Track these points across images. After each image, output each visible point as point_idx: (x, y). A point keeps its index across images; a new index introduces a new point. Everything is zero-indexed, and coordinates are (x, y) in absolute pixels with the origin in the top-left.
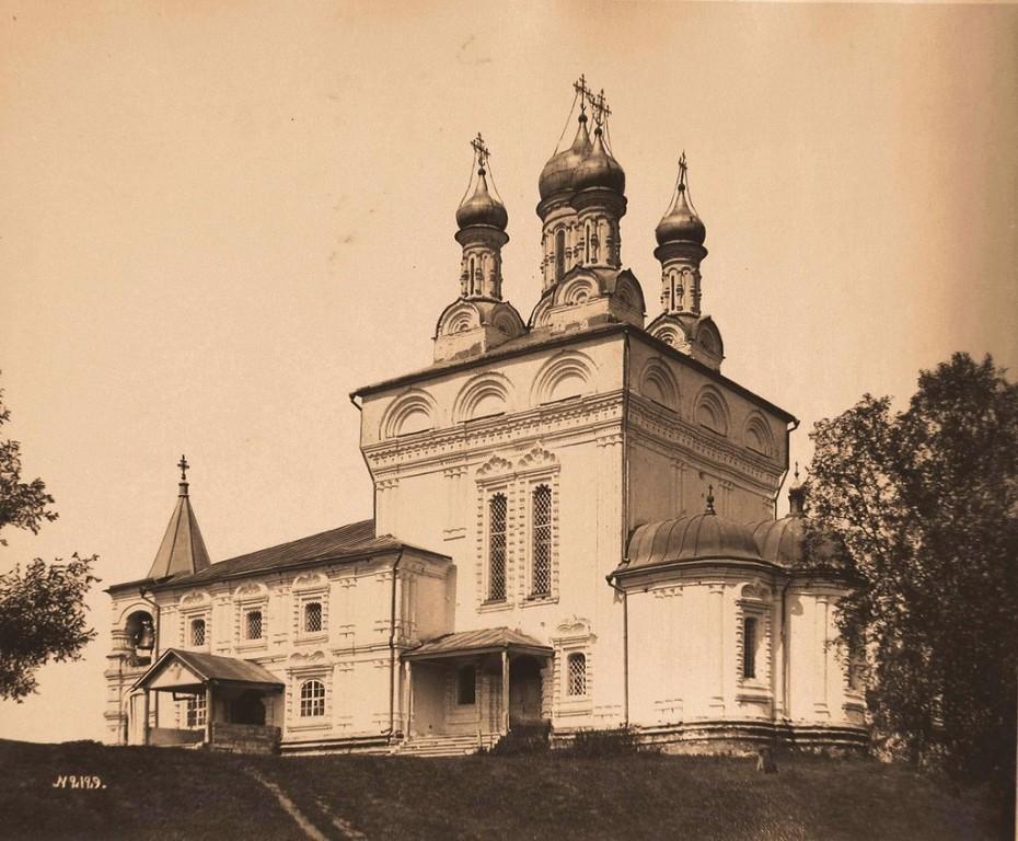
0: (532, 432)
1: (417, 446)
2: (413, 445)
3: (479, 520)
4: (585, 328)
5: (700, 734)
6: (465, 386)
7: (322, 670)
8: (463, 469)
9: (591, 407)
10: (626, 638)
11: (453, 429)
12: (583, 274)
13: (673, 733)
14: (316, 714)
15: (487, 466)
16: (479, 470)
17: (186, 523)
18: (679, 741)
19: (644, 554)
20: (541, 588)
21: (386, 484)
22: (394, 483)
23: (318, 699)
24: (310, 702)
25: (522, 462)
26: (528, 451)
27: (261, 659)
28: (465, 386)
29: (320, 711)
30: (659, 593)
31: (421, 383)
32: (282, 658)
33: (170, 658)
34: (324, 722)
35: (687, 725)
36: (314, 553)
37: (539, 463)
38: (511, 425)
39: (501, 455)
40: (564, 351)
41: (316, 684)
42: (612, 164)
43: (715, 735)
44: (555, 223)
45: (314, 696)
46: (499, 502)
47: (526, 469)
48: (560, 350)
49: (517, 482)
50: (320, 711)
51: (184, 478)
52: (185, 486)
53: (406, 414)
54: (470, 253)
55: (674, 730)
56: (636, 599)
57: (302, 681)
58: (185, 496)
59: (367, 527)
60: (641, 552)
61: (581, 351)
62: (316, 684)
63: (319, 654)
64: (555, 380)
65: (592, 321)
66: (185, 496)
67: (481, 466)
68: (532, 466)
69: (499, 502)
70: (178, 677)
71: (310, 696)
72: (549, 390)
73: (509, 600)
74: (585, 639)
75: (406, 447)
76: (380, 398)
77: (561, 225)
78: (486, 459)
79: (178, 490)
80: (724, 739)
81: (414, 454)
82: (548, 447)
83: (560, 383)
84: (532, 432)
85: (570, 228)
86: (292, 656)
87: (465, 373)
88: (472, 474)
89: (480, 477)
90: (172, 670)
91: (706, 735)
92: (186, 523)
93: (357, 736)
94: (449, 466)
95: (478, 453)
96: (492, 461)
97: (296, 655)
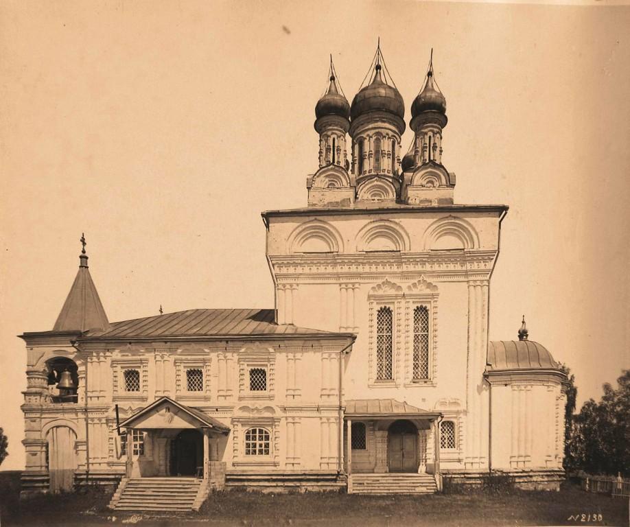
0: (419, 268)
1: (288, 263)
2: (315, 262)
3: (370, 323)
4: (435, 205)
5: (542, 478)
6: (365, 226)
7: (273, 421)
8: (357, 285)
9: (340, 261)
10: (490, 414)
11: (354, 255)
12: (434, 168)
13: (526, 476)
14: (261, 452)
15: (379, 286)
16: (373, 288)
17: (83, 290)
18: (531, 482)
19: (501, 361)
20: (422, 373)
21: (288, 286)
22: (295, 286)
23: (263, 442)
24: (255, 446)
25: (409, 287)
26: (380, 281)
27: (204, 408)
28: (365, 226)
29: (265, 450)
30: (515, 388)
31: (329, 217)
32: (230, 409)
33: (164, 403)
34: (272, 460)
35: (535, 472)
36: (176, 329)
37: (422, 290)
38: (403, 260)
39: (393, 281)
40: (316, 219)
41: (261, 431)
42: (443, 105)
43: (550, 479)
44: (374, 131)
45: (258, 438)
46: (385, 313)
47: (376, 293)
48: (448, 214)
49: (403, 301)
50: (265, 450)
51: (84, 252)
52: (84, 258)
53: (306, 238)
54: (333, 133)
55: (527, 474)
56: (500, 392)
57: (247, 428)
58: (84, 265)
59: (268, 316)
60: (498, 359)
61: (331, 223)
62: (261, 431)
63: (269, 409)
64: (439, 235)
65: (440, 201)
66: (84, 265)
67: (375, 285)
68: (415, 291)
69: (385, 313)
70: (171, 421)
71: (254, 438)
72: (436, 238)
73: (398, 382)
74: (458, 412)
75: (285, 262)
76: (359, 219)
77: (377, 134)
78: (380, 281)
79: (78, 262)
80: (554, 481)
81: (374, 267)
82: (397, 281)
83: (441, 238)
84: (419, 268)
85: (385, 137)
86: (240, 409)
87: (367, 216)
88: (366, 288)
89: (372, 293)
90: (162, 415)
91: (546, 479)
92: (83, 290)
93: (307, 473)
94: (348, 281)
95: (371, 276)
96: (383, 283)
97: (244, 408)
